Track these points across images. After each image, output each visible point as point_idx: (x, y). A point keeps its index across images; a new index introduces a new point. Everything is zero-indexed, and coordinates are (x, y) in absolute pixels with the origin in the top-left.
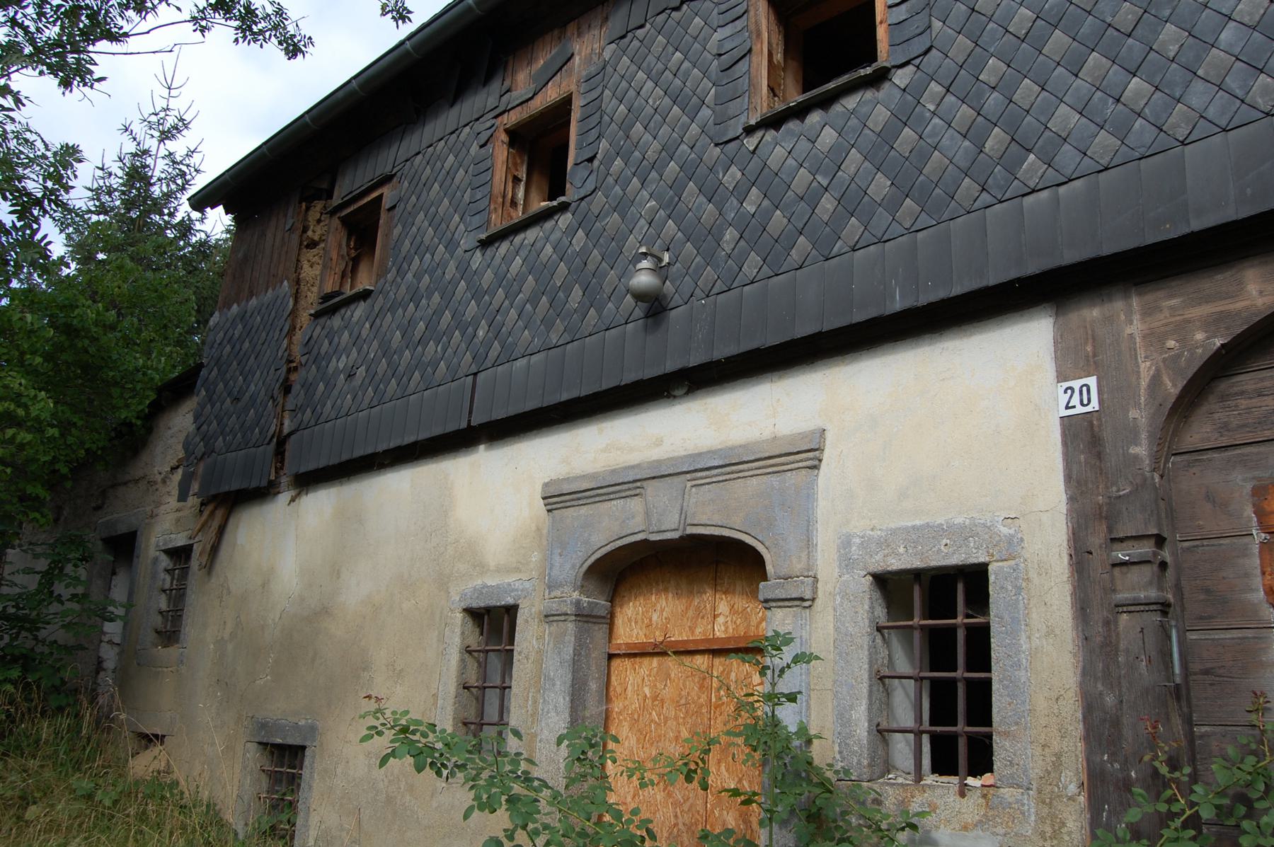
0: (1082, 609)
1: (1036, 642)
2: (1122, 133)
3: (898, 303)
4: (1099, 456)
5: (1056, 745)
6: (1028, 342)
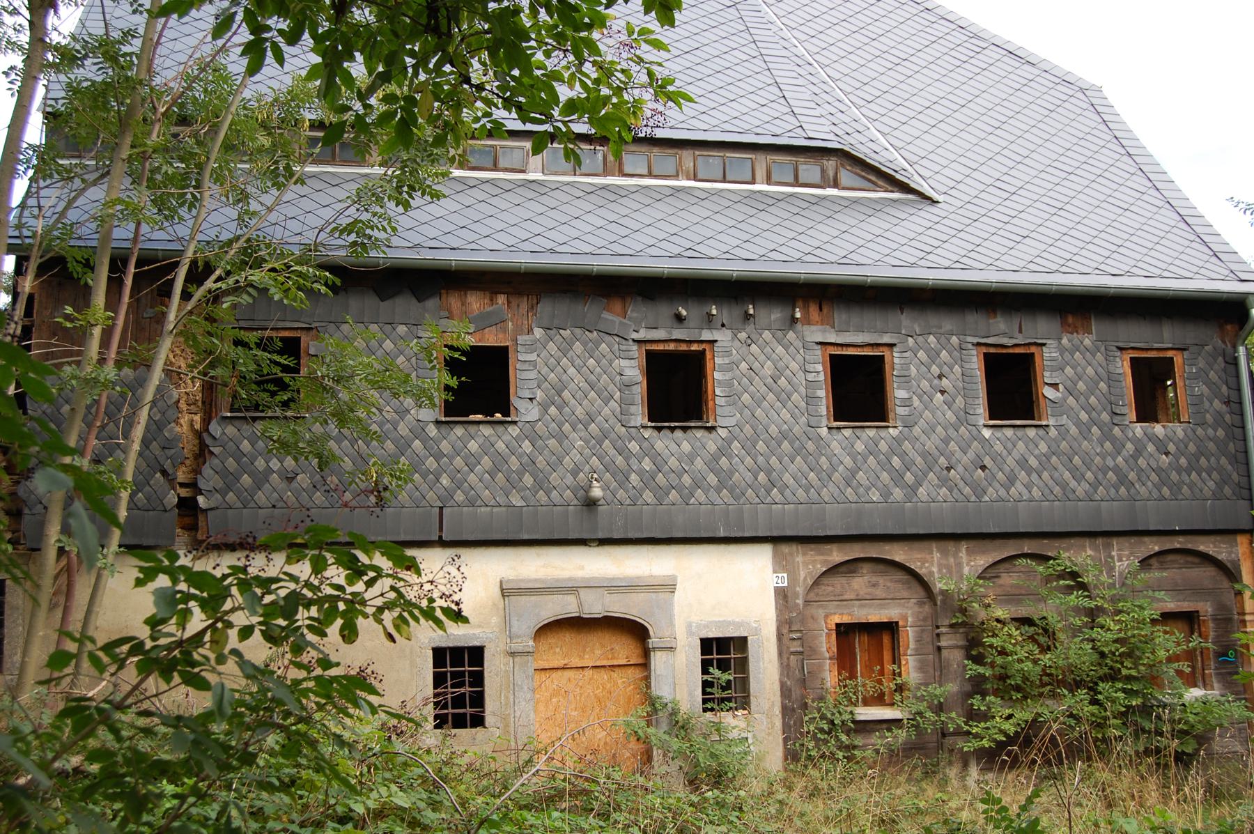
0: (780, 654)
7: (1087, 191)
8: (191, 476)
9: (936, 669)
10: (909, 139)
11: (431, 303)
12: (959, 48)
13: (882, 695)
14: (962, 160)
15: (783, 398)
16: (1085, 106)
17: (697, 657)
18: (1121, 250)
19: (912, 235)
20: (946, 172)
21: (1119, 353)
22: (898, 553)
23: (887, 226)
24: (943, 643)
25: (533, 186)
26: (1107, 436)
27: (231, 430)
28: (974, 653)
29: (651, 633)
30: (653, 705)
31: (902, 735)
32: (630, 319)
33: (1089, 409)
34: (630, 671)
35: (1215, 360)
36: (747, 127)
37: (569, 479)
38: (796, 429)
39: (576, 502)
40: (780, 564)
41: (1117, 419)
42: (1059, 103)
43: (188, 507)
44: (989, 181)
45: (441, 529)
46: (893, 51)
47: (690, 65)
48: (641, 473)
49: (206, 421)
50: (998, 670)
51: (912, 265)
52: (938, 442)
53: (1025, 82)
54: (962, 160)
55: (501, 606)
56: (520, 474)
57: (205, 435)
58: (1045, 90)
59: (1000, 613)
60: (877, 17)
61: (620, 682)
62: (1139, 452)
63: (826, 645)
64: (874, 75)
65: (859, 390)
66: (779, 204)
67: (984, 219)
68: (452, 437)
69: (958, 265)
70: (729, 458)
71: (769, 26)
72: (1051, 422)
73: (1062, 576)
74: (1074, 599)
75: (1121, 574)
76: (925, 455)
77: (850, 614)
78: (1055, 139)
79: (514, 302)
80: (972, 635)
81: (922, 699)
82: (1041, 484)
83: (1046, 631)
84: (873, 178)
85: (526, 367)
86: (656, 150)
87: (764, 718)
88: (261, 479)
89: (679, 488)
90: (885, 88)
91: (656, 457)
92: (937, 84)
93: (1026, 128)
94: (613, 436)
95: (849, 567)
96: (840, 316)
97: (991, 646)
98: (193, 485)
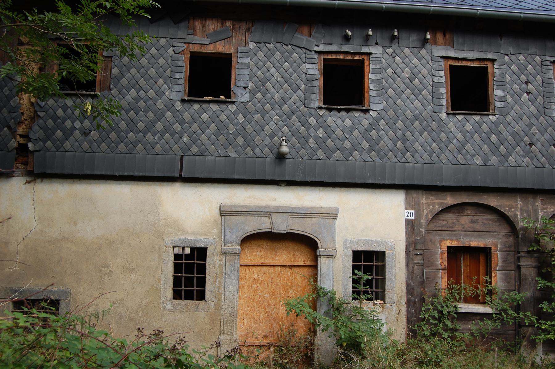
0: (407, 264)
1: (397, 271)
2: (430, 155)
3: (370, 181)
4: (413, 229)
5: (400, 294)
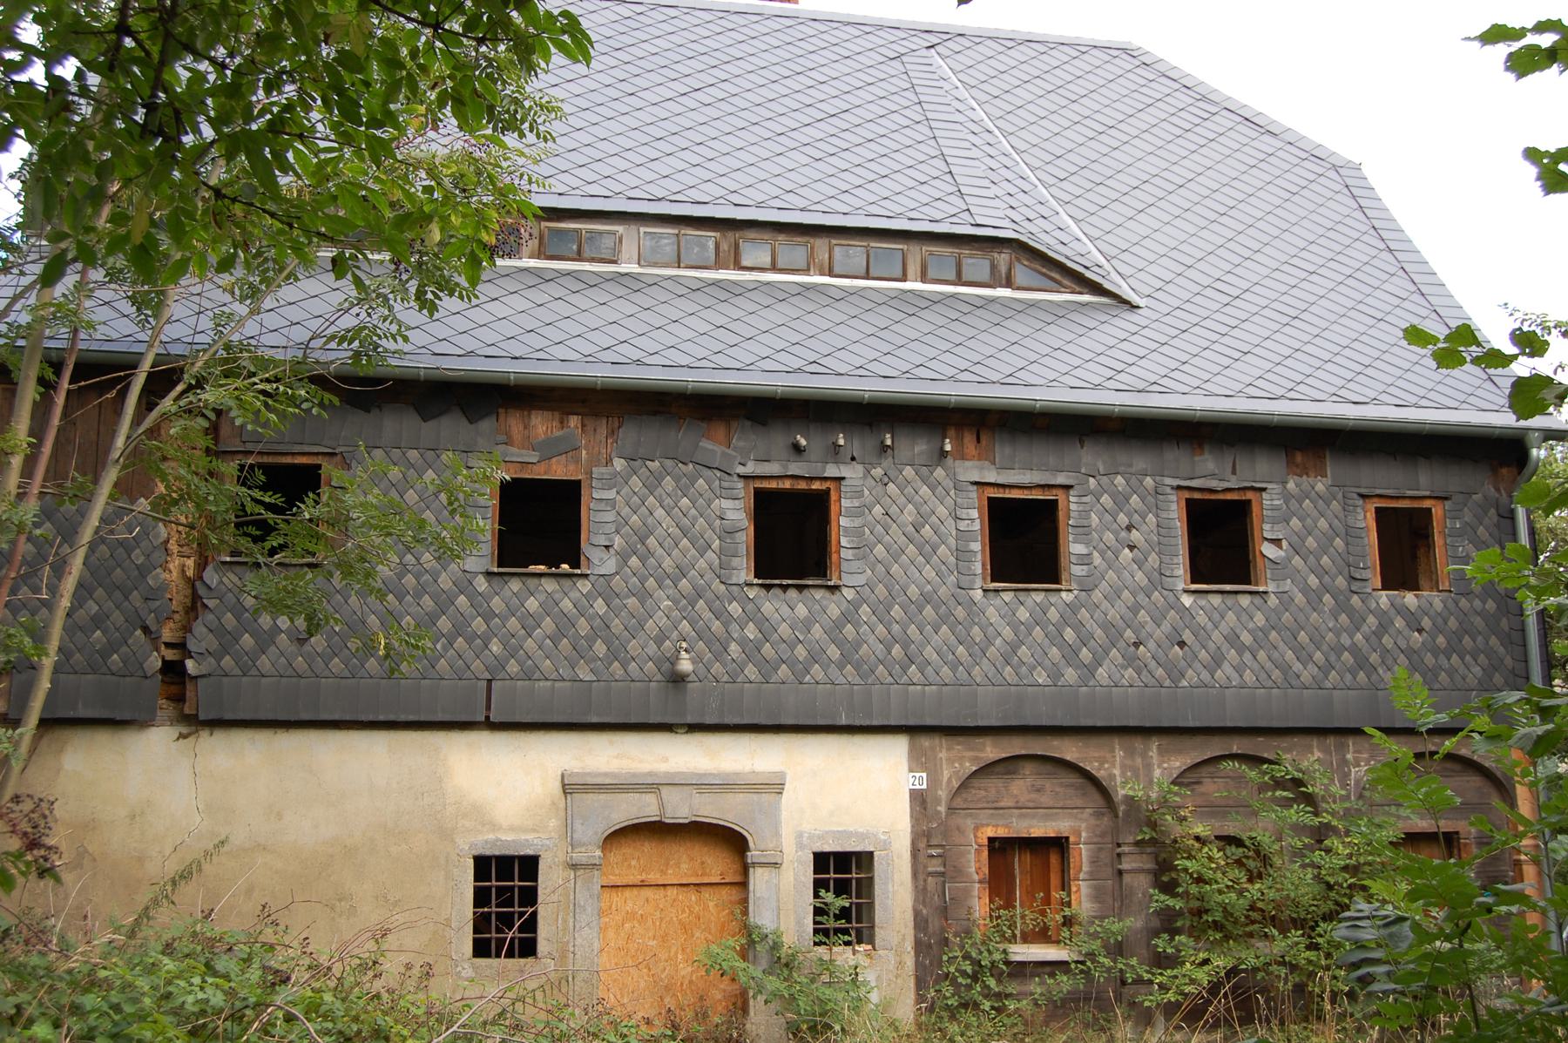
0: (915, 875)
2: (954, 669)
6: (898, 747)
7: (1332, 295)
8: (180, 634)
9: (1115, 898)
10: (1108, 227)
11: (486, 425)
12: (1182, 114)
13: (1045, 929)
14: (1174, 254)
15: (927, 551)
16: (1337, 187)
17: (808, 876)
18: (1369, 371)
19: (1101, 348)
20: (1153, 269)
21: (1361, 502)
22: (1069, 750)
23: (1071, 336)
24: (1125, 866)
25: (624, 280)
26: (1342, 606)
27: (231, 578)
28: (1165, 879)
29: (751, 844)
30: (751, 941)
31: (1065, 983)
32: (735, 449)
33: (1320, 572)
34: (725, 891)
35: (1486, 513)
36: (899, 209)
37: (652, 648)
38: (943, 591)
39: (659, 677)
40: (917, 760)
41: (1355, 586)
42: (1304, 183)
43: (173, 672)
44: (1206, 281)
45: (488, 708)
46: (1098, 116)
47: (835, 131)
48: (743, 642)
49: (201, 566)
50: (1195, 904)
51: (1096, 387)
52: (1124, 610)
53: (1262, 156)
54: (1174, 254)
55: (562, 805)
56: (590, 641)
57: (198, 584)
58: (1287, 167)
59: (1199, 829)
60: (1079, 73)
61: (711, 904)
62: (1384, 627)
63: (975, 864)
64: (1070, 146)
65: (1024, 542)
66: (935, 307)
67: (1196, 330)
68: (506, 593)
69: (1156, 388)
70: (856, 626)
71: (941, 83)
72: (1271, 587)
73: (1278, 784)
74: (1297, 814)
75: (1357, 782)
76: (1107, 626)
77: (1006, 826)
78: (1295, 229)
79: (590, 422)
80: (1163, 855)
81: (1095, 936)
82: (1256, 666)
83: (1258, 852)
84: (1057, 276)
85: (602, 506)
86: (781, 237)
87: (891, 955)
88: (266, 640)
89: (792, 663)
90: (1083, 163)
91: (763, 623)
92: (1151, 158)
93: (1259, 214)
94: (709, 594)
95: (1008, 765)
96: (1003, 450)
97: (1186, 870)
98: (181, 646)
